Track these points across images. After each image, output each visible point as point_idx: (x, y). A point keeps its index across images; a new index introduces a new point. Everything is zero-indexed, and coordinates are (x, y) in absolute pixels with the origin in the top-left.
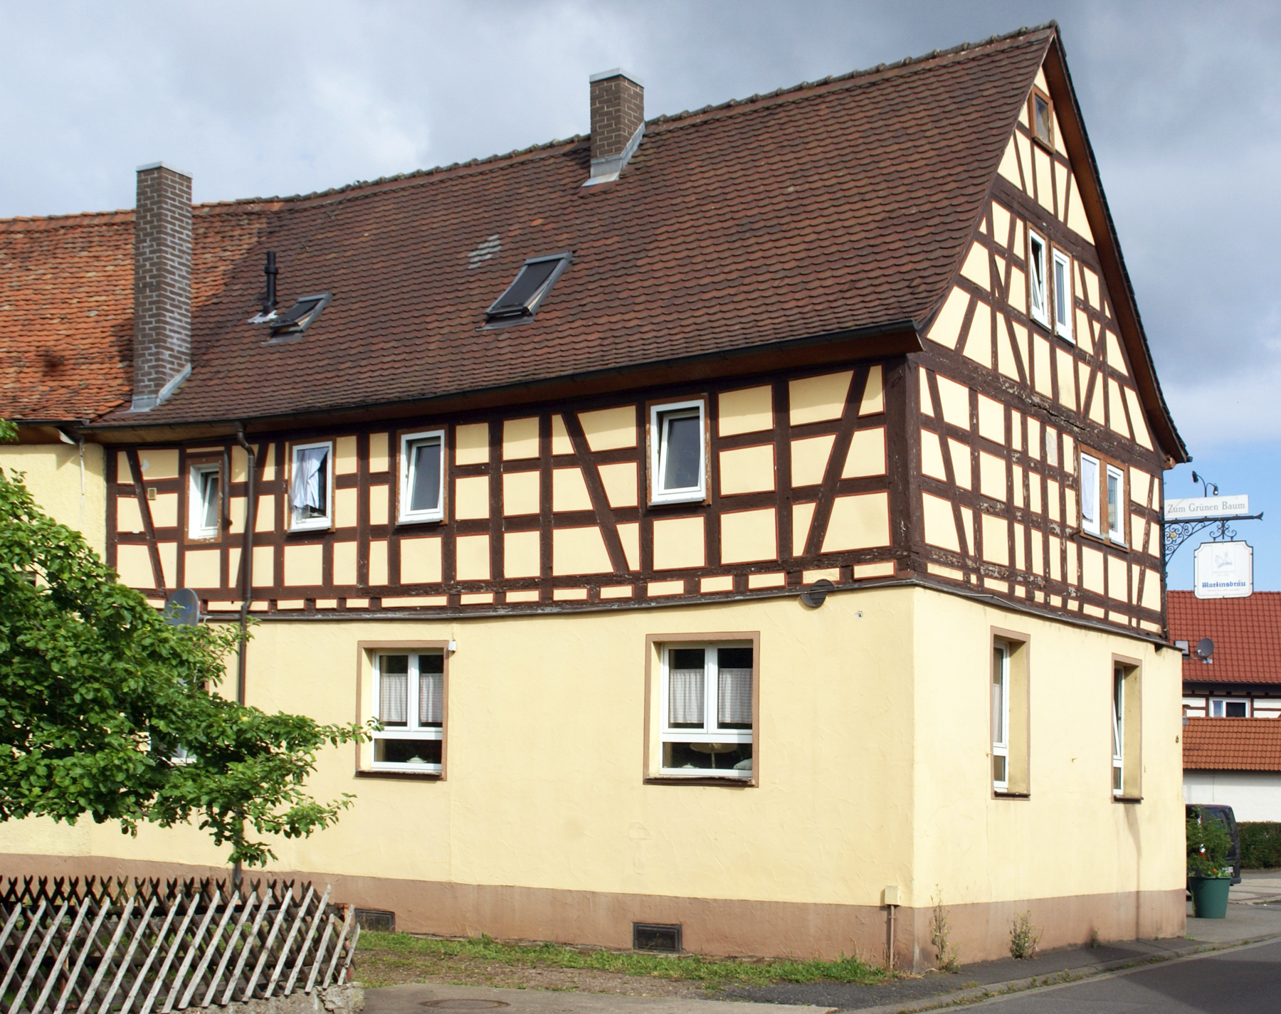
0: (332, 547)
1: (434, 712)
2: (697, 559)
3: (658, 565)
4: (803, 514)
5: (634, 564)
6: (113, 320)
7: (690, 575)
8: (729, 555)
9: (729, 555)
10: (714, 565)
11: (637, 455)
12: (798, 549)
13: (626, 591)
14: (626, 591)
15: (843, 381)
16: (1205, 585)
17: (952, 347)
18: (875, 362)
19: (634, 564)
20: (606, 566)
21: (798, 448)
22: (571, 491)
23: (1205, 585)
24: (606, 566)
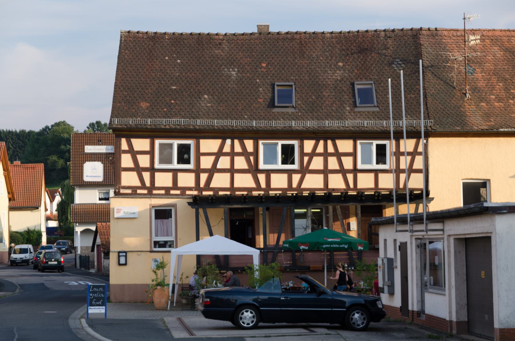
0: (288, 185)
1: (457, 316)
2: (170, 184)
3: (157, 185)
4: (204, 177)
5: (148, 184)
6: (281, 273)
7: (167, 189)
8: (180, 184)
9: (180, 184)
10: (175, 186)
11: (354, 155)
12: (202, 185)
13: (145, 192)
14: (145, 192)
15: (219, 142)
16: (87, 176)
17: (202, 141)
18: (229, 138)
19: (148, 184)
20: (138, 184)
21: (321, 167)
22: (333, 163)
23: (87, 176)
24: (138, 184)
